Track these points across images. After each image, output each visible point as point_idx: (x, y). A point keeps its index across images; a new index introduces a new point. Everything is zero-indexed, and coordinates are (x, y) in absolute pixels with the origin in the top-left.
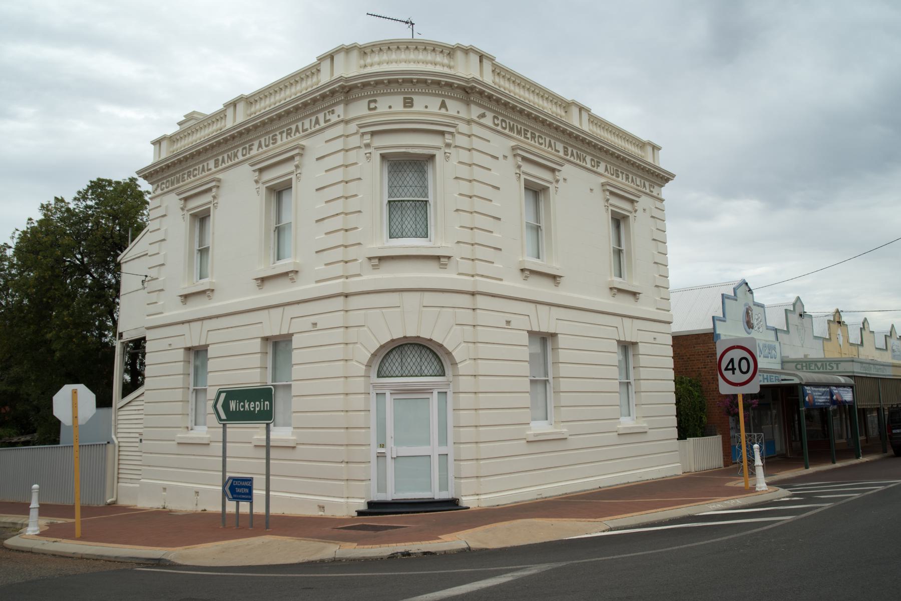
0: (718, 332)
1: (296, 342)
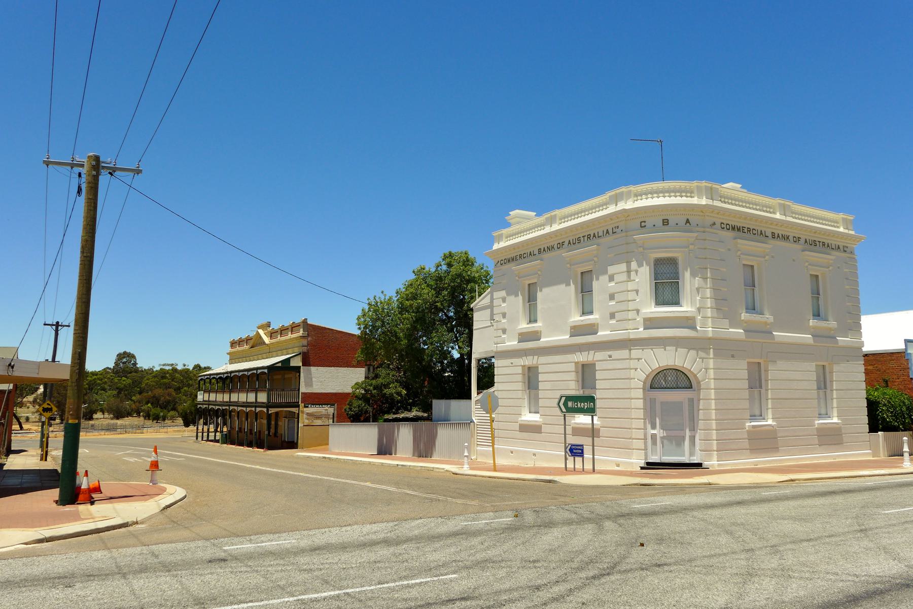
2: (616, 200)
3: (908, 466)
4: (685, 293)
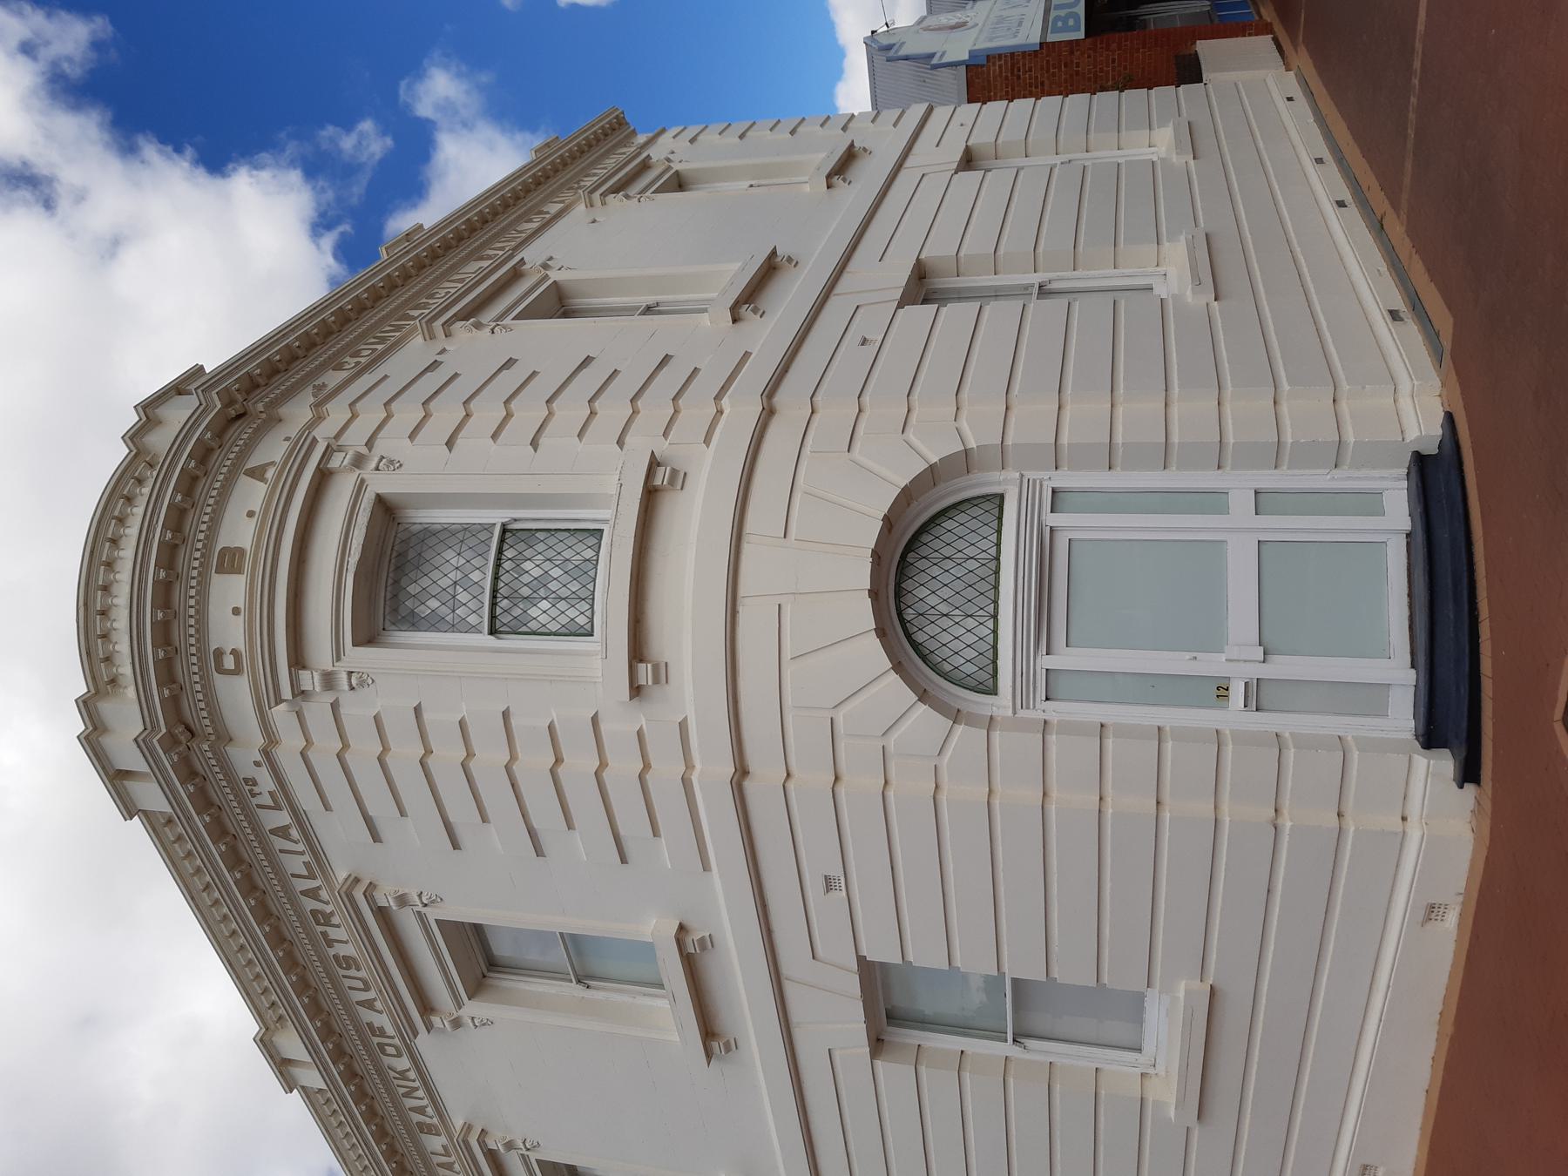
0: (966, 57)
1: (882, 951)
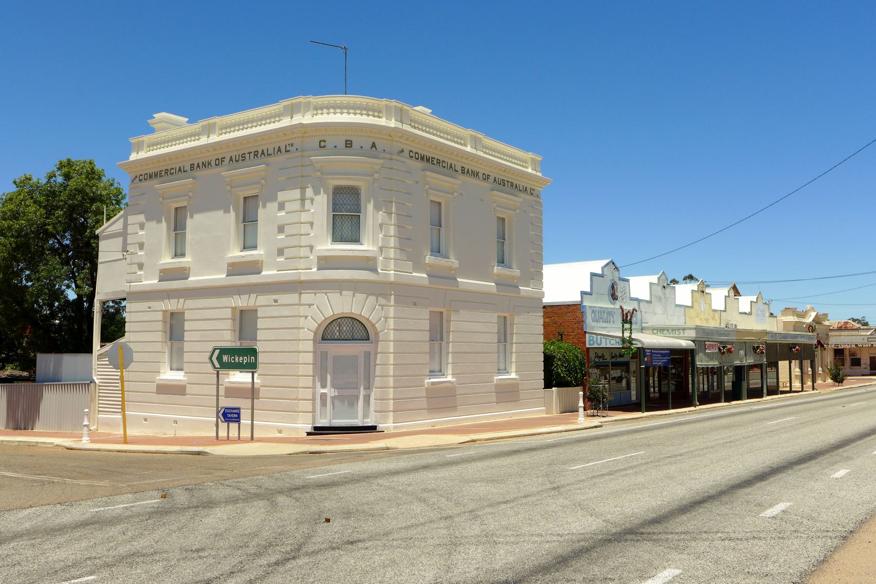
0: (584, 304)
2: (292, 111)
3: (582, 421)
4: (366, 230)
